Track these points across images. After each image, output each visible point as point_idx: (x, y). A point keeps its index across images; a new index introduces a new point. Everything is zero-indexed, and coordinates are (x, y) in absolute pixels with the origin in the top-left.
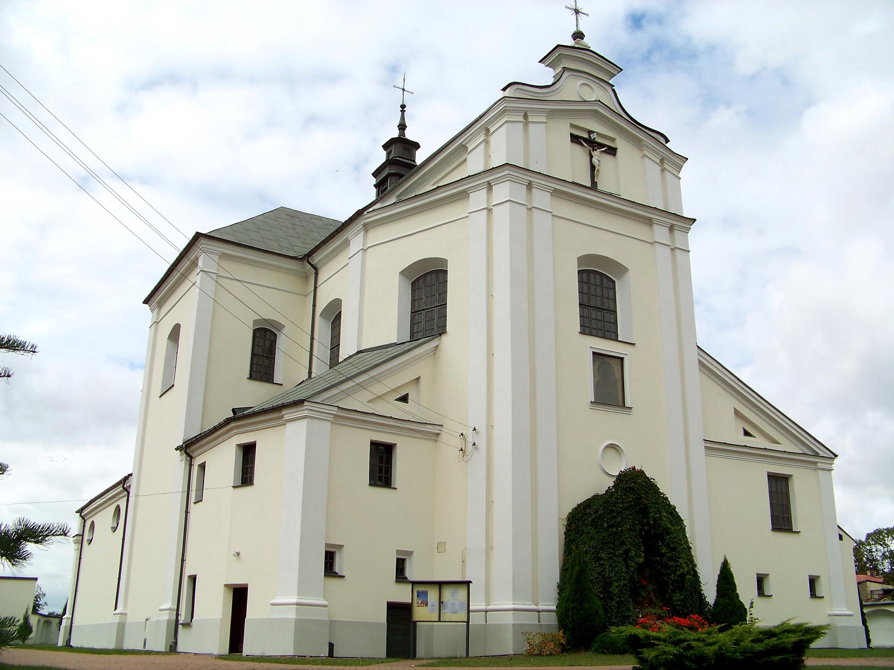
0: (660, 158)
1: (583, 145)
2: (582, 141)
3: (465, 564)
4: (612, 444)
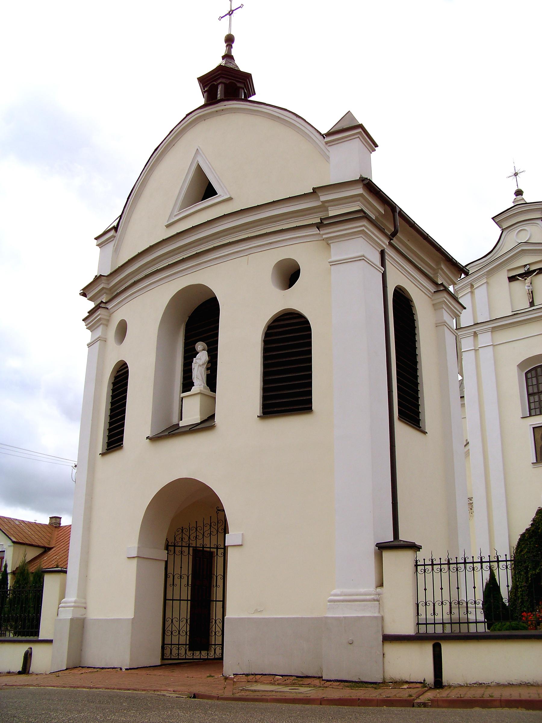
1: (518, 279)
3: (198, 694)
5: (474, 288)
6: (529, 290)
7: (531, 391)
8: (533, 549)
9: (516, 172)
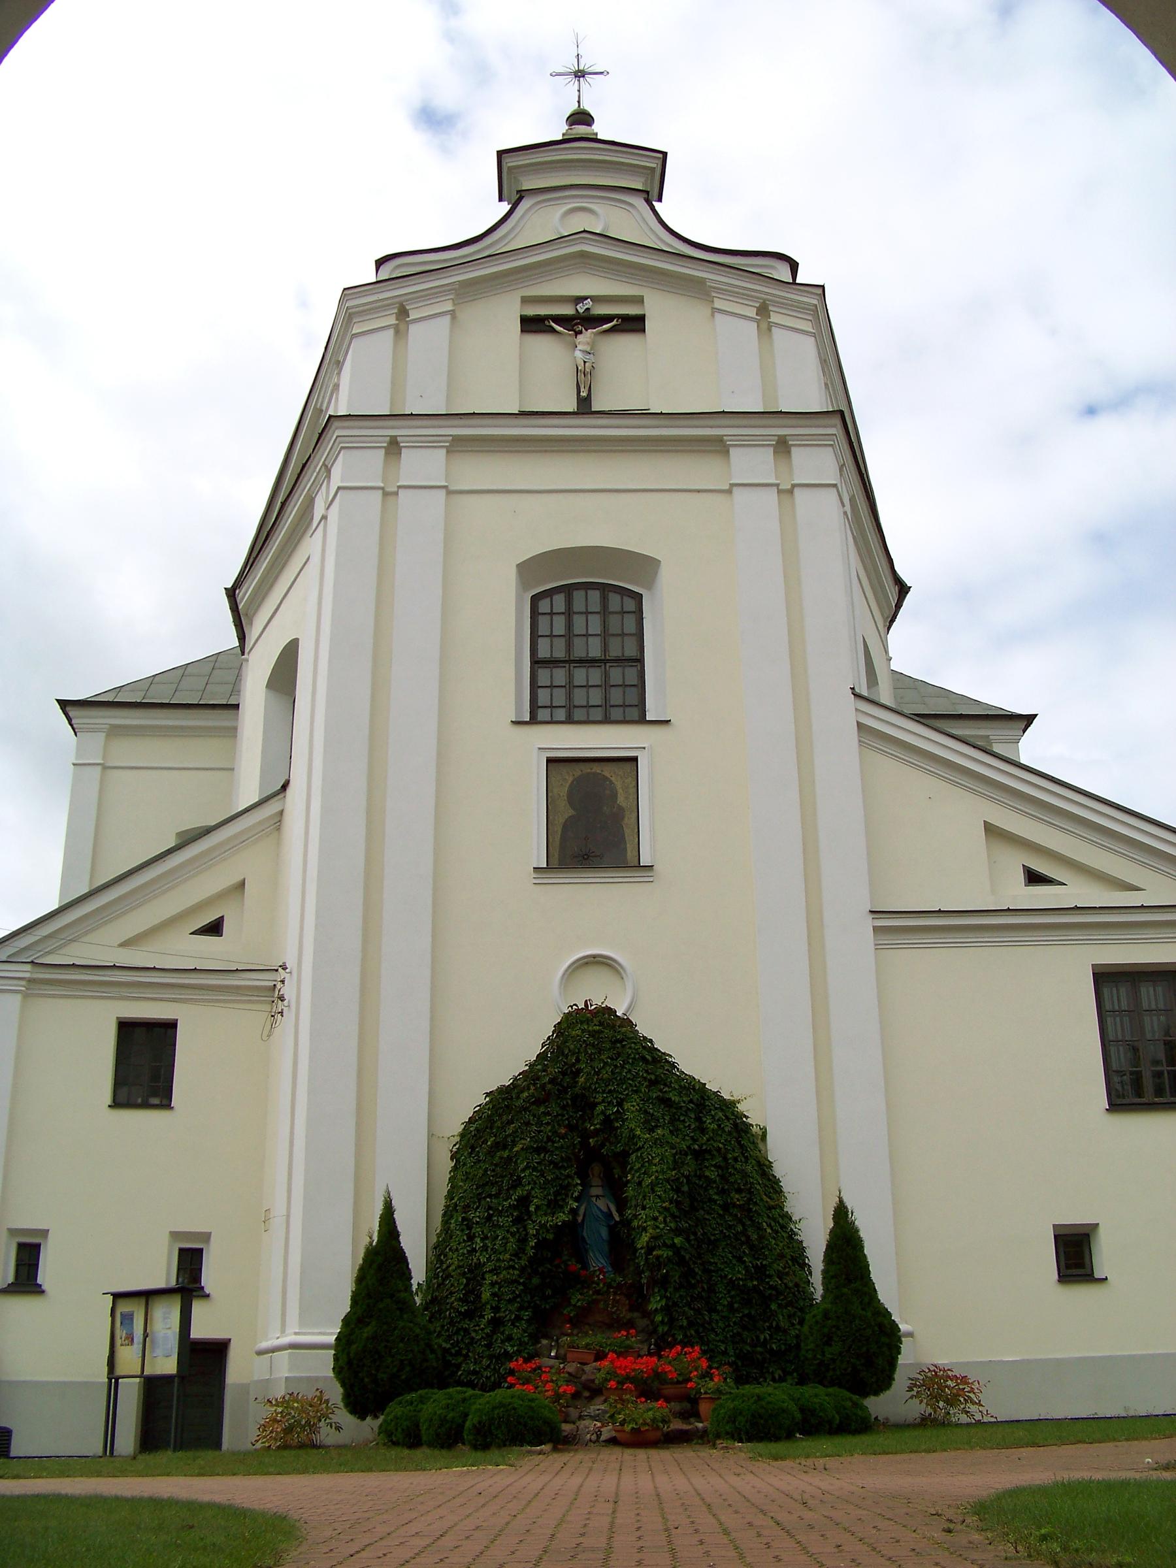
0: (757, 305)
1: (554, 331)
2: (553, 324)
4: (594, 956)
5: (408, 319)
6: (587, 364)
7: (544, 652)
8: (549, 1139)
9: (581, 68)
